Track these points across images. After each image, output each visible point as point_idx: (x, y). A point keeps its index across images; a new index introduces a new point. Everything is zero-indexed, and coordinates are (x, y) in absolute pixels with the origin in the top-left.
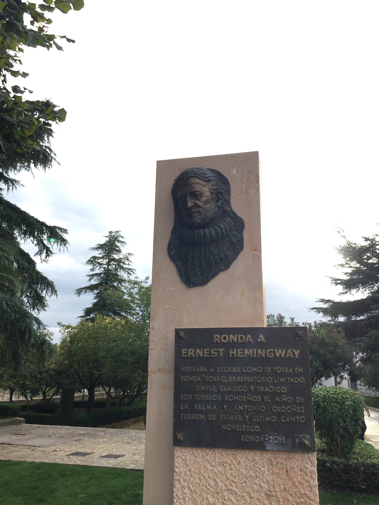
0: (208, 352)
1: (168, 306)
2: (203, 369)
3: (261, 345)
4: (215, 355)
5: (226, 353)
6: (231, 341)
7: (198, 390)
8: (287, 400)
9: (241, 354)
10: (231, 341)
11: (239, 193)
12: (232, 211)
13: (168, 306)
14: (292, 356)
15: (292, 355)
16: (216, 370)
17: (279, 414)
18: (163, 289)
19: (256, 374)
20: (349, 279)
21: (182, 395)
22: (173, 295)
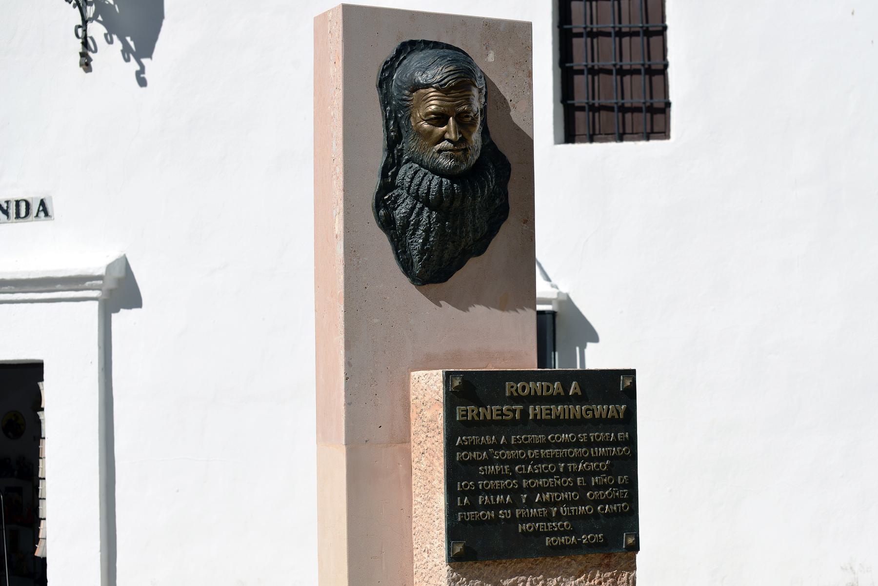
0: (499, 412)
1: (376, 321)
2: (491, 439)
3: (577, 399)
4: (509, 416)
5: (524, 413)
6: (532, 393)
7: (485, 473)
8: (561, 482)
9: (497, 415)
10: (532, 393)
11: (499, 103)
12: (652, 132)
13: (376, 321)
14: (617, 417)
15: (615, 414)
16: (508, 439)
17: (596, 502)
18: (366, 286)
19: (566, 445)
20: (526, 307)
21: (459, 483)
22: (385, 298)
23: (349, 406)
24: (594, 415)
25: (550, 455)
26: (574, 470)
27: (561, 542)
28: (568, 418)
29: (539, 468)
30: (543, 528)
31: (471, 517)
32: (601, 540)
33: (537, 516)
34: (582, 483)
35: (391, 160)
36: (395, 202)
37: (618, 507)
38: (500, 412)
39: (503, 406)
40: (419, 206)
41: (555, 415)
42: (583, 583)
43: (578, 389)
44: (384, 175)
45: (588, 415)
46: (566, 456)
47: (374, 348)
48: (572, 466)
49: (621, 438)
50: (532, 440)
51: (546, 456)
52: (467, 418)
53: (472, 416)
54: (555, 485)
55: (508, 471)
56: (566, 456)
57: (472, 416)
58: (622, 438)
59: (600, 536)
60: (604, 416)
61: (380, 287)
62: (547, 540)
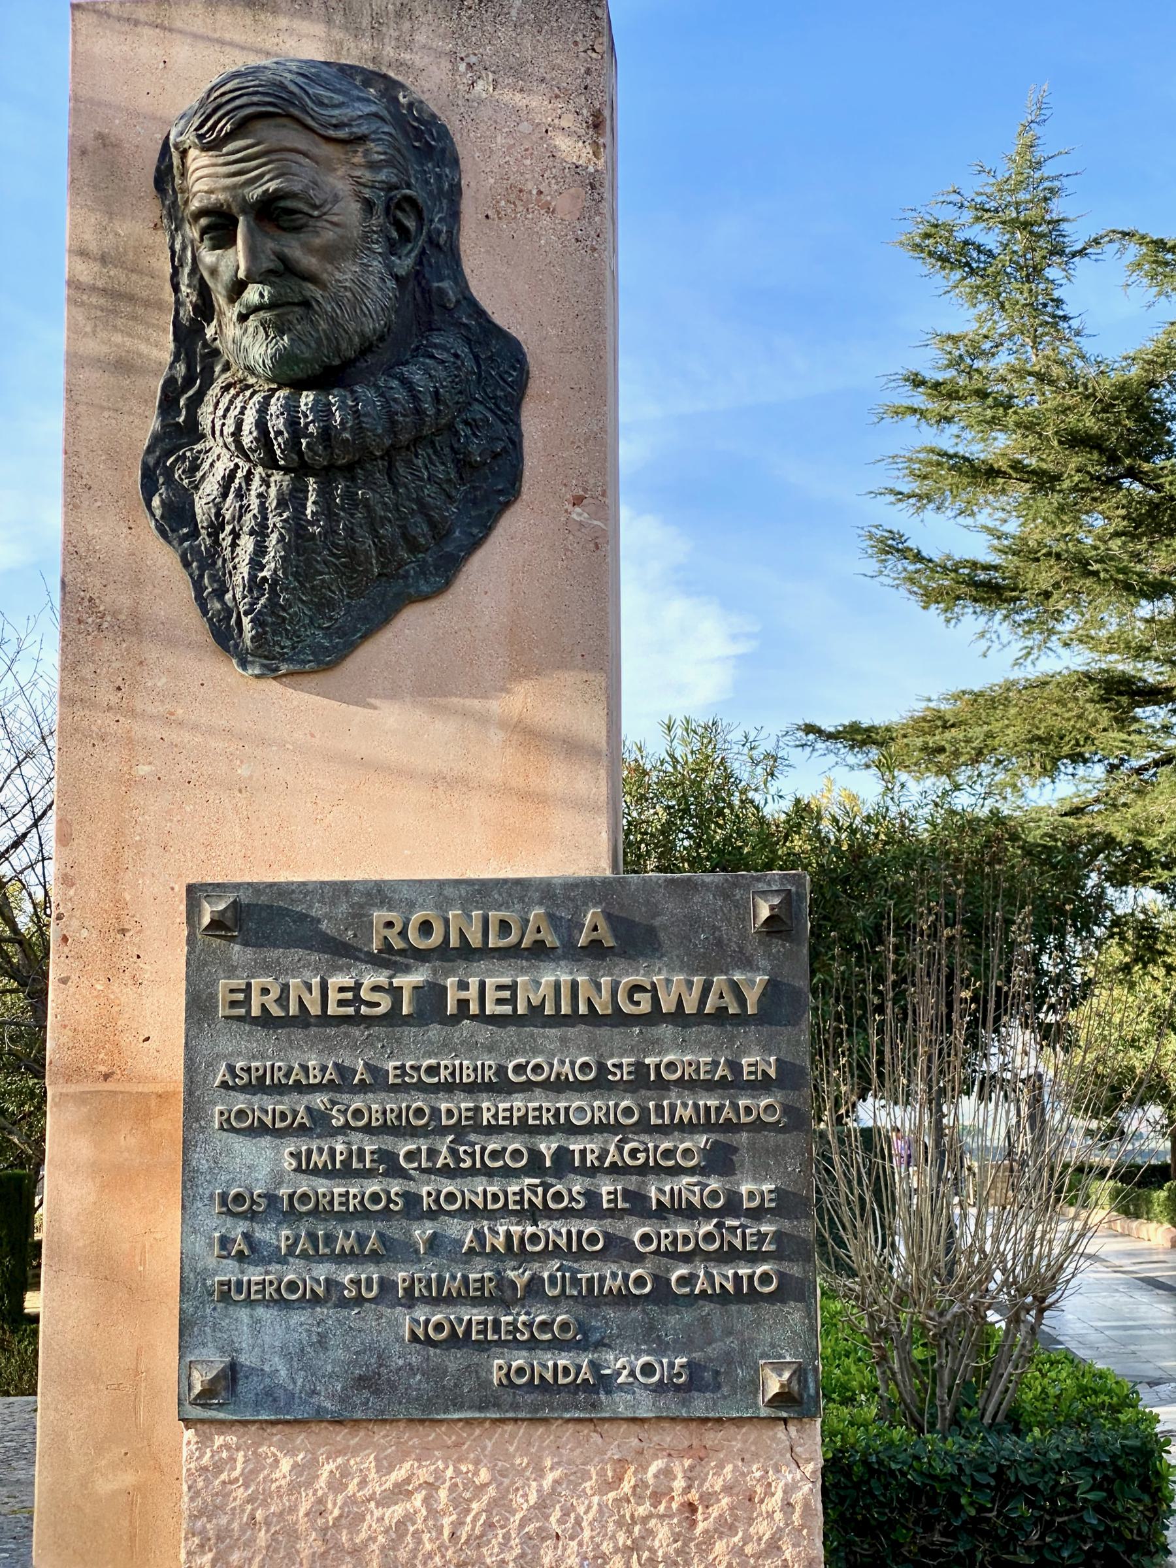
9: (341, 1003)
18: (119, 682)
23: (62, 986)
24: (656, 1001)
25: (511, 1118)
26: (589, 1164)
27: (541, 1377)
28: (569, 1012)
29: (472, 1155)
30: (484, 1332)
31: (252, 1291)
32: (679, 1375)
33: (463, 1293)
34: (615, 1201)
35: (181, 369)
36: (194, 468)
37: (737, 1278)
38: (509, 993)
39: (713, 976)
40: (245, 466)
41: (526, 1004)
42: (629, 1502)
43: (603, 925)
44: (168, 404)
45: (638, 1003)
46: (562, 1121)
47: (138, 838)
48: (583, 1153)
49: (750, 1073)
50: (453, 1074)
51: (497, 1120)
52: (515, 1009)
53: (263, 1005)
54: (526, 1206)
55: (372, 1161)
56: (562, 1121)
57: (263, 1005)
58: (755, 1073)
59: (678, 1361)
60: (690, 1008)
61: (159, 684)
62: (495, 1370)
